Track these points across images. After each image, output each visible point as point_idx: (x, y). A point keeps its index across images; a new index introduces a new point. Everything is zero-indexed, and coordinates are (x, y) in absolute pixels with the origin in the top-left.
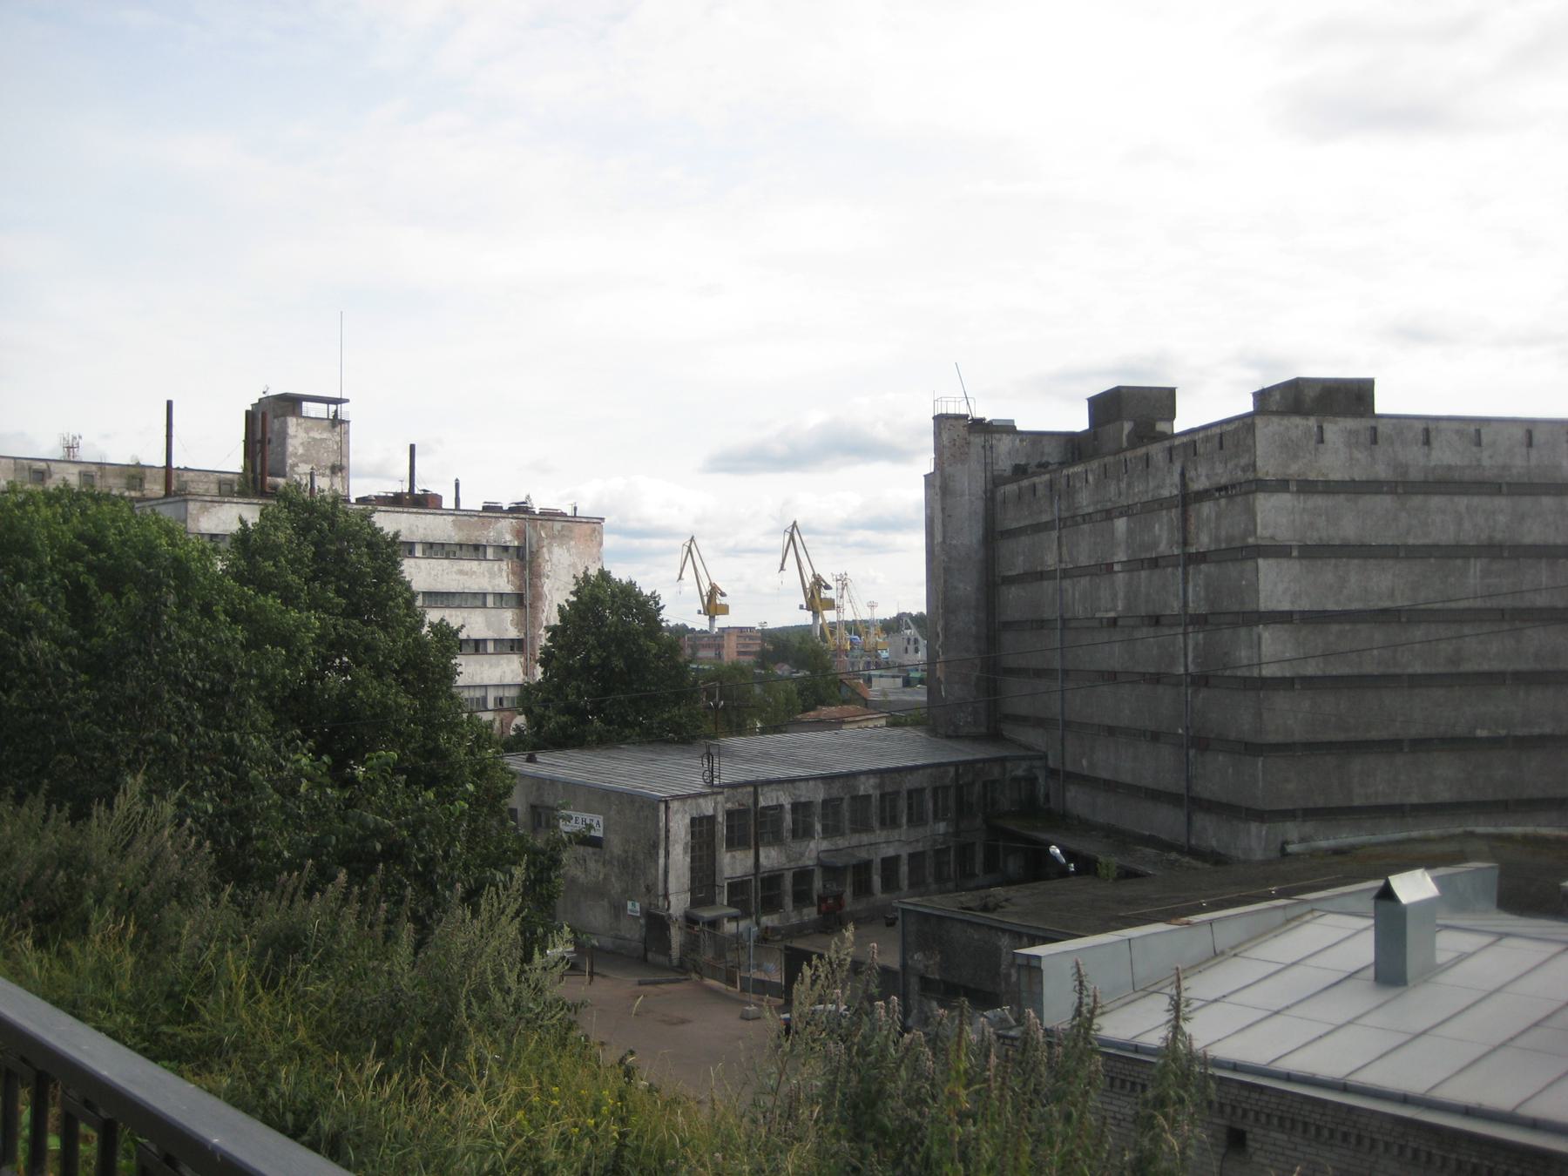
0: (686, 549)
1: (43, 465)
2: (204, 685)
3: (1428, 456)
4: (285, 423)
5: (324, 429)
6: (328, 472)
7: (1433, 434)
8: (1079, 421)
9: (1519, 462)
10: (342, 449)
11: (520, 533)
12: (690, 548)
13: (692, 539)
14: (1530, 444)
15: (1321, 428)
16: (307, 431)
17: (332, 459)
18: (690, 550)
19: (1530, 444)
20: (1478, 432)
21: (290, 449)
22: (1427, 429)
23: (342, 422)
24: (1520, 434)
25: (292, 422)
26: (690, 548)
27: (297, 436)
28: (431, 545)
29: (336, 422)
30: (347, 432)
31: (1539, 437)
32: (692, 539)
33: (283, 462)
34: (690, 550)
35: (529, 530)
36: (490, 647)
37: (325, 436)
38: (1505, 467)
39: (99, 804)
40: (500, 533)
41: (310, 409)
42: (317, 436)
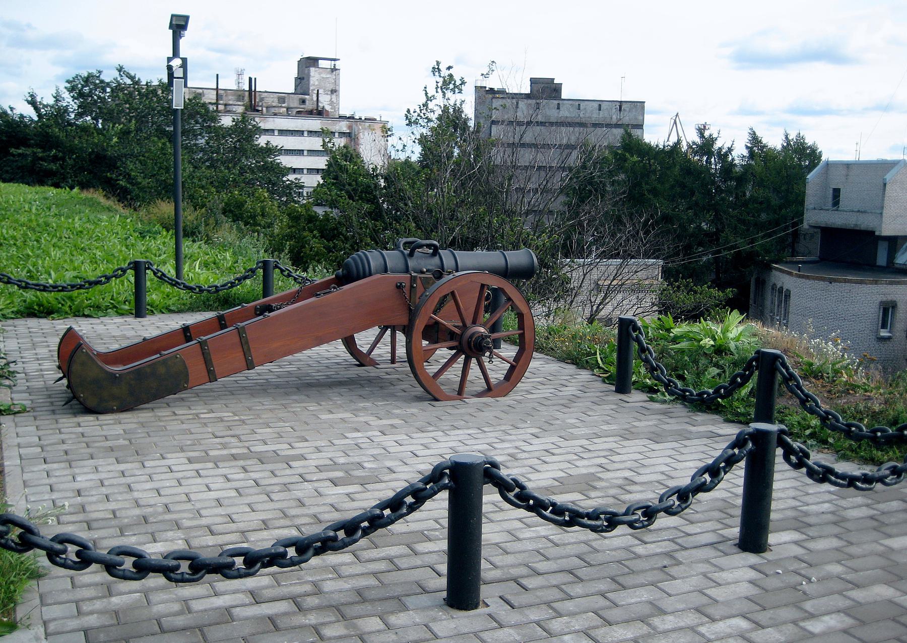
0: (673, 121)
1: (201, 91)
2: (383, 202)
3: (559, 113)
4: (309, 70)
5: (328, 73)
6: (329, 93)
7: (561, 106)
8: (526, 90)
9: (595, 115)
10: (336, 82)
11: (350, 127)
12: (675, 121)
13: (677, 115)
14: (600, 109)
15: (517, 103)
16: (320, 74)
17: (331, 87)
18: (675, 122)
19: (600, 109)
20: (600, 105)
21: (311, 82)
22: (578, 103)
23: (337, 69)
24: (596, 105)
25: (312, 69)
26: (675, 121)
27: (315, 75)
28: (311, 132)
29: (334, 70)
30: (339, 74)
31: (604, 106)
32: (677, 115)
33: (309, 89)
34: (675, 122)
35: (354, 126)
36: (305, 171)
37: (328, 76)
38: (590, 118)
39: (795, 488)
40: (341, 127)
41: (322, 63)
42: (324, 76)
